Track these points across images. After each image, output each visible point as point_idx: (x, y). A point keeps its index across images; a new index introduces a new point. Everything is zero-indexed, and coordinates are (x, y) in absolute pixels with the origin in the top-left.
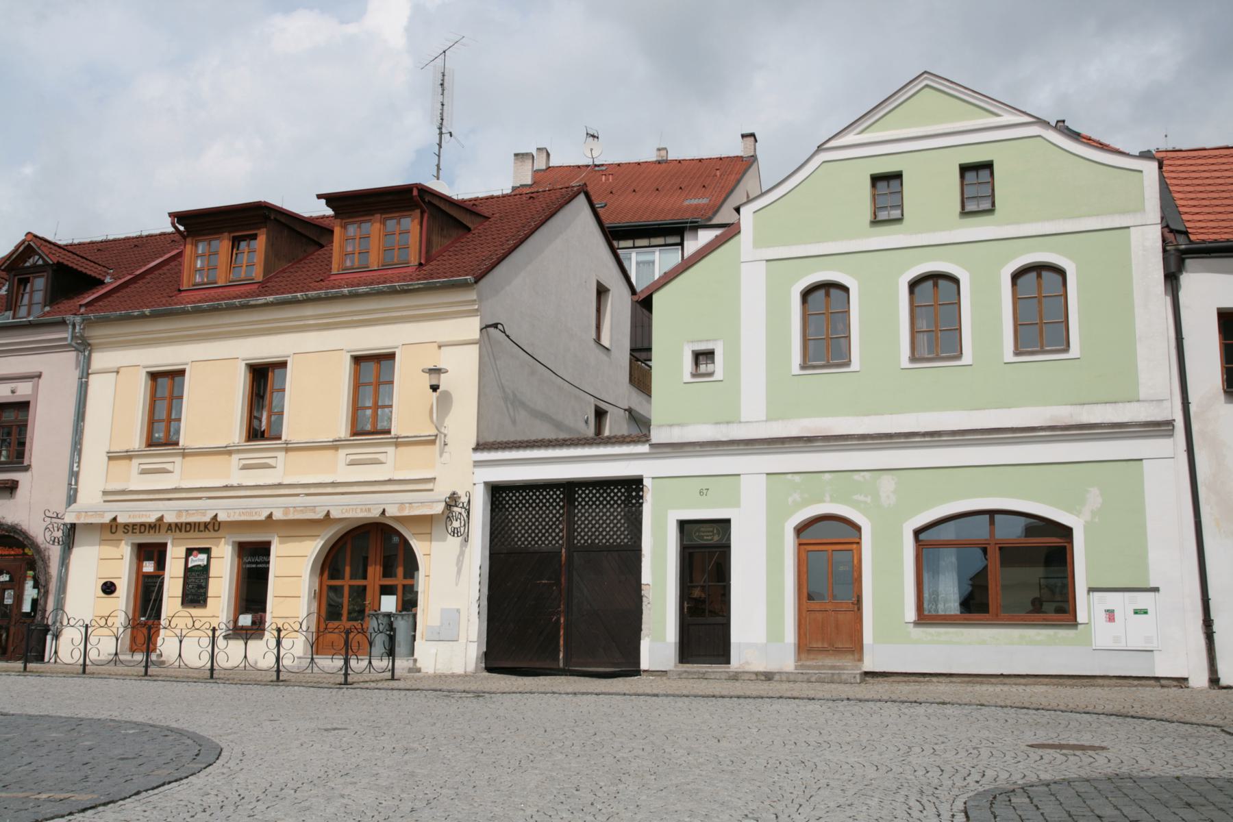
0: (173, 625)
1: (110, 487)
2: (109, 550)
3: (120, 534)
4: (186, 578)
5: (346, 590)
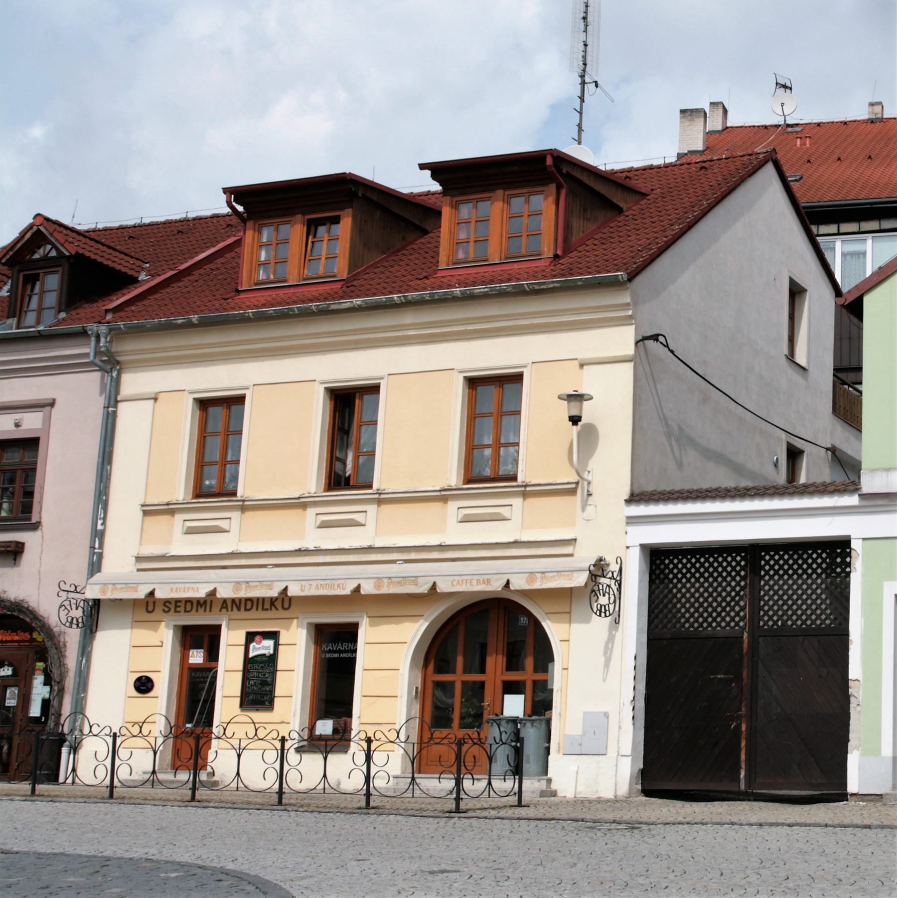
0: (229, 733)
1: (146, 551)
2: (144, 635)
3: (158, 613)
4: (246, 671)
5: (456, 723)
